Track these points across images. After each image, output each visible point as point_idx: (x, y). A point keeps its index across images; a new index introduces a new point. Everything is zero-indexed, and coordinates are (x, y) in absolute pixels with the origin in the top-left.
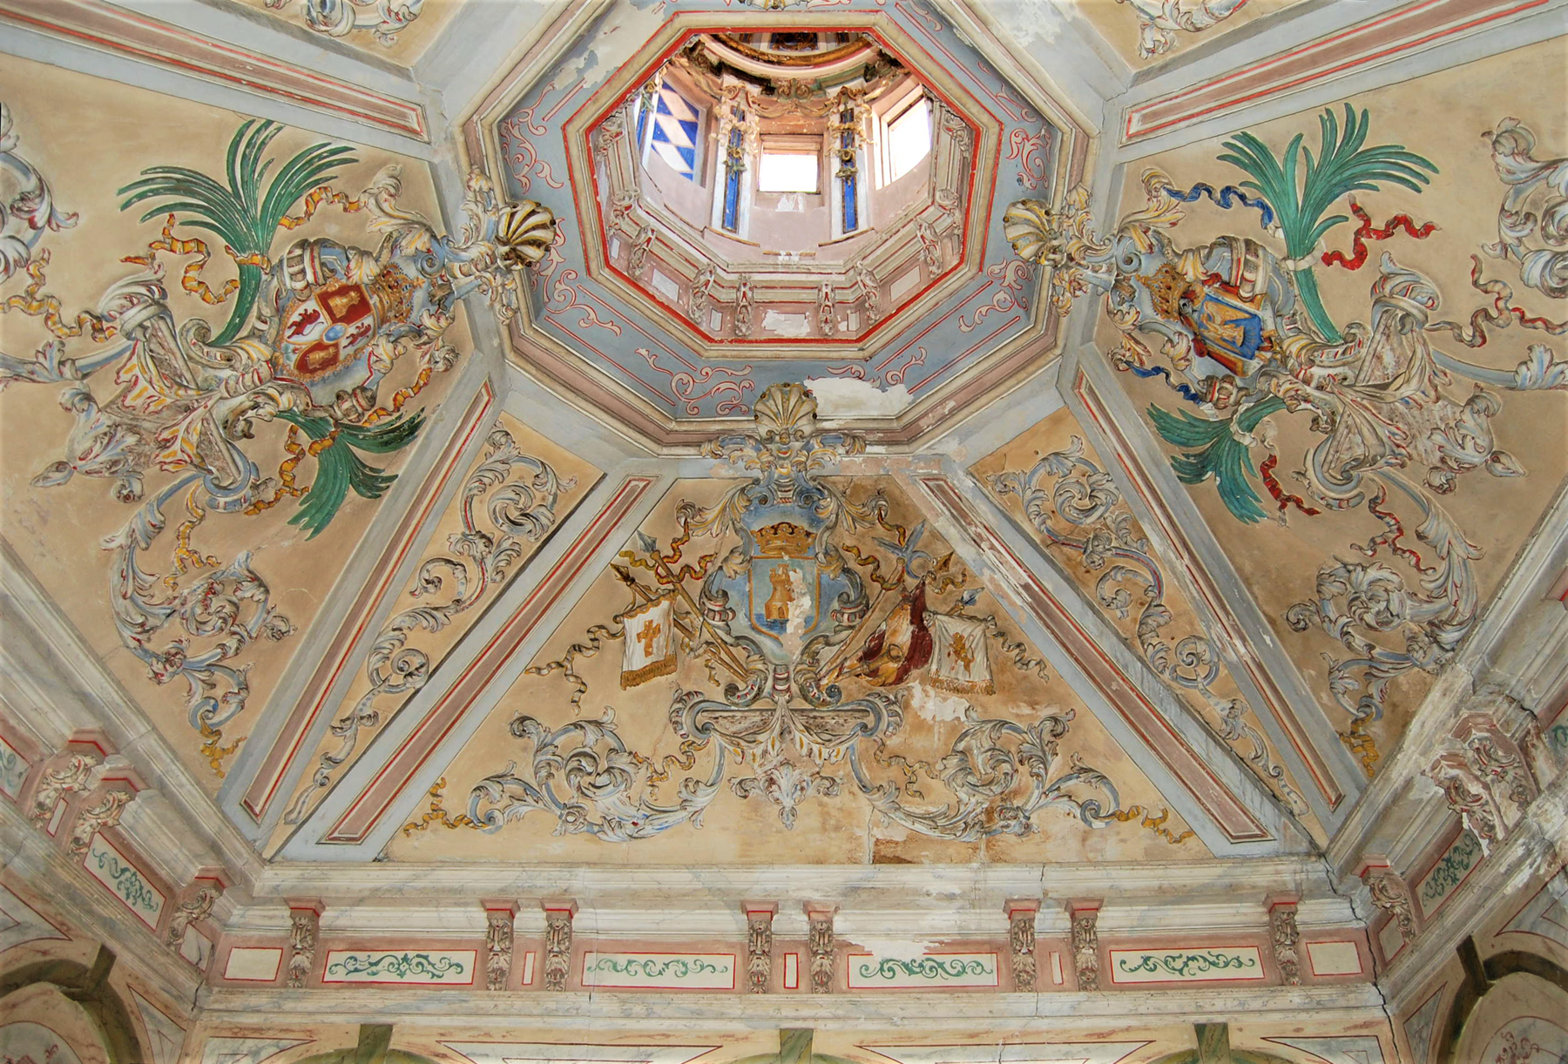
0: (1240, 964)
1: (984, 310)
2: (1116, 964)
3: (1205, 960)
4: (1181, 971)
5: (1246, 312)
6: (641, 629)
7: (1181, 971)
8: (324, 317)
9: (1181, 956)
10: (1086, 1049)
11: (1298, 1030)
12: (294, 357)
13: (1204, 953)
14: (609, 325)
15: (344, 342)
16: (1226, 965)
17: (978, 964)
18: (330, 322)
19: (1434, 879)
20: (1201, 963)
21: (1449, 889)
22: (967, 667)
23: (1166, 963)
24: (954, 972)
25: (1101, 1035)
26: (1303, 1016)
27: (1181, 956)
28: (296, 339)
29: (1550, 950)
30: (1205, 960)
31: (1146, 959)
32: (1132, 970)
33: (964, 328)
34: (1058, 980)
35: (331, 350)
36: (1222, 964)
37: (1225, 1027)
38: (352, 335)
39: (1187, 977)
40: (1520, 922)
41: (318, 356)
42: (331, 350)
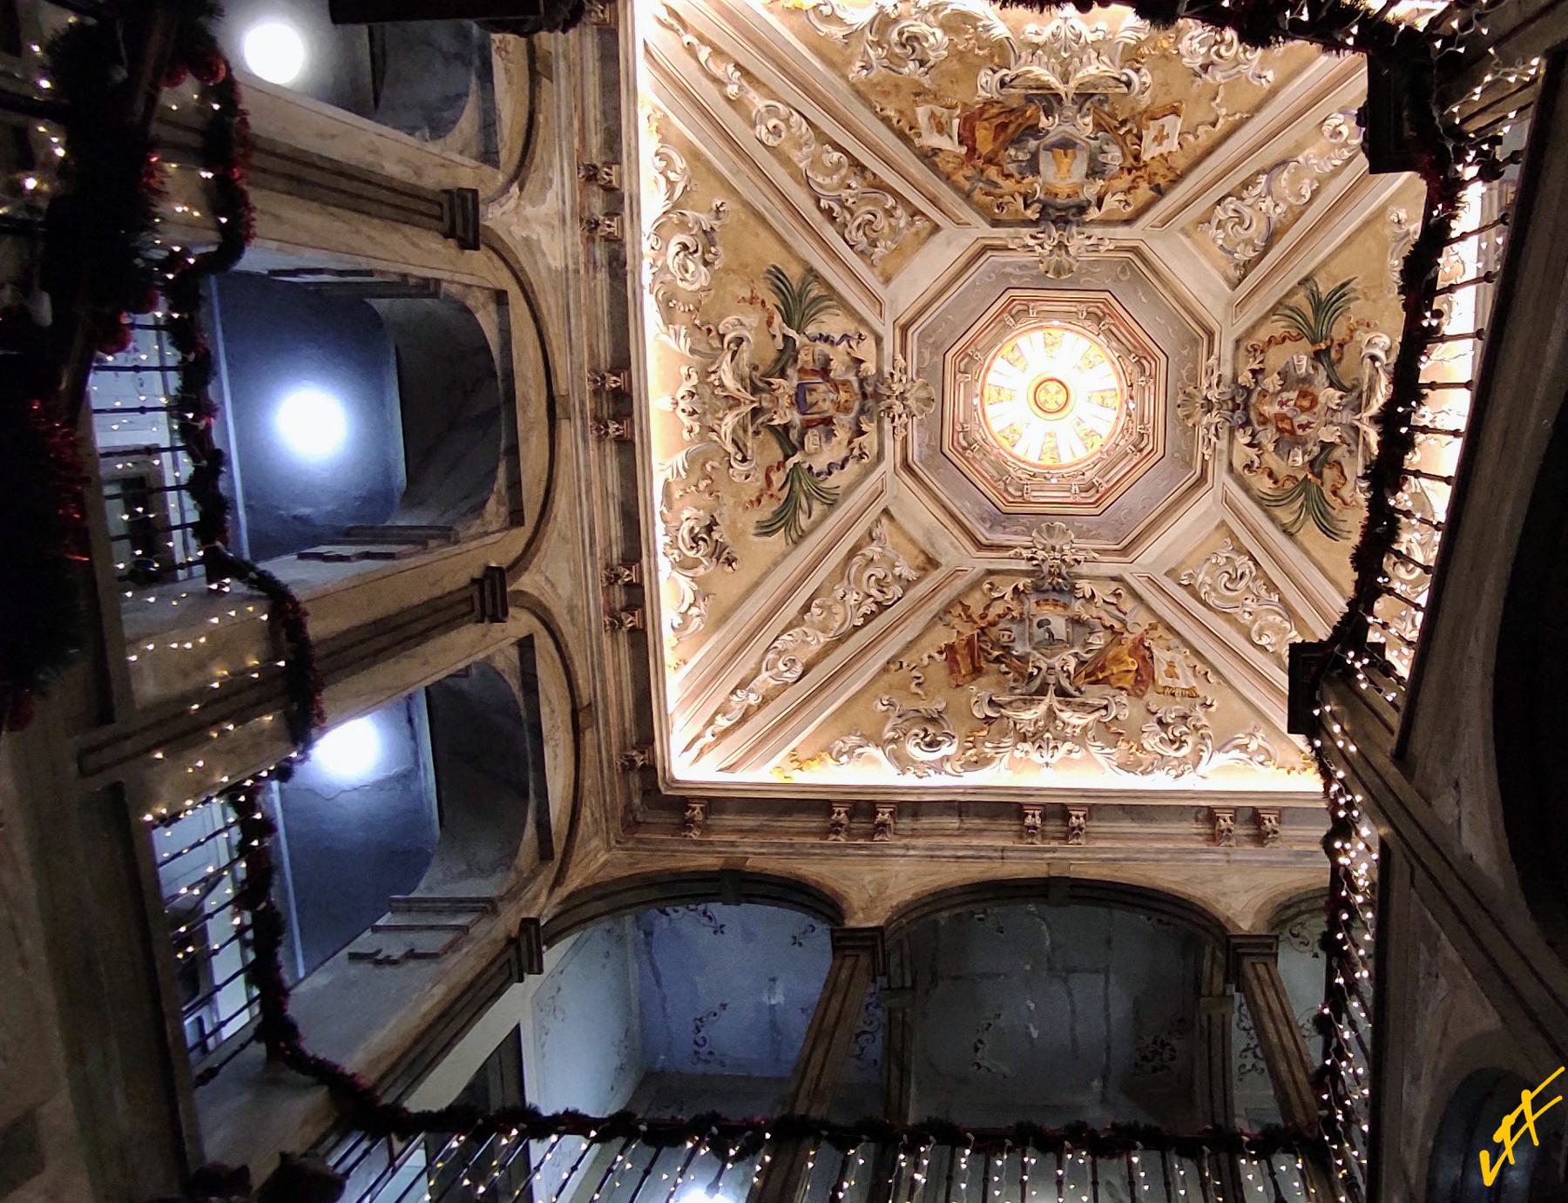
6: (1165, 142)
8: (1296, 424)
12: (1316, 410)
15: (1291, 403)
41: (1306, 403)
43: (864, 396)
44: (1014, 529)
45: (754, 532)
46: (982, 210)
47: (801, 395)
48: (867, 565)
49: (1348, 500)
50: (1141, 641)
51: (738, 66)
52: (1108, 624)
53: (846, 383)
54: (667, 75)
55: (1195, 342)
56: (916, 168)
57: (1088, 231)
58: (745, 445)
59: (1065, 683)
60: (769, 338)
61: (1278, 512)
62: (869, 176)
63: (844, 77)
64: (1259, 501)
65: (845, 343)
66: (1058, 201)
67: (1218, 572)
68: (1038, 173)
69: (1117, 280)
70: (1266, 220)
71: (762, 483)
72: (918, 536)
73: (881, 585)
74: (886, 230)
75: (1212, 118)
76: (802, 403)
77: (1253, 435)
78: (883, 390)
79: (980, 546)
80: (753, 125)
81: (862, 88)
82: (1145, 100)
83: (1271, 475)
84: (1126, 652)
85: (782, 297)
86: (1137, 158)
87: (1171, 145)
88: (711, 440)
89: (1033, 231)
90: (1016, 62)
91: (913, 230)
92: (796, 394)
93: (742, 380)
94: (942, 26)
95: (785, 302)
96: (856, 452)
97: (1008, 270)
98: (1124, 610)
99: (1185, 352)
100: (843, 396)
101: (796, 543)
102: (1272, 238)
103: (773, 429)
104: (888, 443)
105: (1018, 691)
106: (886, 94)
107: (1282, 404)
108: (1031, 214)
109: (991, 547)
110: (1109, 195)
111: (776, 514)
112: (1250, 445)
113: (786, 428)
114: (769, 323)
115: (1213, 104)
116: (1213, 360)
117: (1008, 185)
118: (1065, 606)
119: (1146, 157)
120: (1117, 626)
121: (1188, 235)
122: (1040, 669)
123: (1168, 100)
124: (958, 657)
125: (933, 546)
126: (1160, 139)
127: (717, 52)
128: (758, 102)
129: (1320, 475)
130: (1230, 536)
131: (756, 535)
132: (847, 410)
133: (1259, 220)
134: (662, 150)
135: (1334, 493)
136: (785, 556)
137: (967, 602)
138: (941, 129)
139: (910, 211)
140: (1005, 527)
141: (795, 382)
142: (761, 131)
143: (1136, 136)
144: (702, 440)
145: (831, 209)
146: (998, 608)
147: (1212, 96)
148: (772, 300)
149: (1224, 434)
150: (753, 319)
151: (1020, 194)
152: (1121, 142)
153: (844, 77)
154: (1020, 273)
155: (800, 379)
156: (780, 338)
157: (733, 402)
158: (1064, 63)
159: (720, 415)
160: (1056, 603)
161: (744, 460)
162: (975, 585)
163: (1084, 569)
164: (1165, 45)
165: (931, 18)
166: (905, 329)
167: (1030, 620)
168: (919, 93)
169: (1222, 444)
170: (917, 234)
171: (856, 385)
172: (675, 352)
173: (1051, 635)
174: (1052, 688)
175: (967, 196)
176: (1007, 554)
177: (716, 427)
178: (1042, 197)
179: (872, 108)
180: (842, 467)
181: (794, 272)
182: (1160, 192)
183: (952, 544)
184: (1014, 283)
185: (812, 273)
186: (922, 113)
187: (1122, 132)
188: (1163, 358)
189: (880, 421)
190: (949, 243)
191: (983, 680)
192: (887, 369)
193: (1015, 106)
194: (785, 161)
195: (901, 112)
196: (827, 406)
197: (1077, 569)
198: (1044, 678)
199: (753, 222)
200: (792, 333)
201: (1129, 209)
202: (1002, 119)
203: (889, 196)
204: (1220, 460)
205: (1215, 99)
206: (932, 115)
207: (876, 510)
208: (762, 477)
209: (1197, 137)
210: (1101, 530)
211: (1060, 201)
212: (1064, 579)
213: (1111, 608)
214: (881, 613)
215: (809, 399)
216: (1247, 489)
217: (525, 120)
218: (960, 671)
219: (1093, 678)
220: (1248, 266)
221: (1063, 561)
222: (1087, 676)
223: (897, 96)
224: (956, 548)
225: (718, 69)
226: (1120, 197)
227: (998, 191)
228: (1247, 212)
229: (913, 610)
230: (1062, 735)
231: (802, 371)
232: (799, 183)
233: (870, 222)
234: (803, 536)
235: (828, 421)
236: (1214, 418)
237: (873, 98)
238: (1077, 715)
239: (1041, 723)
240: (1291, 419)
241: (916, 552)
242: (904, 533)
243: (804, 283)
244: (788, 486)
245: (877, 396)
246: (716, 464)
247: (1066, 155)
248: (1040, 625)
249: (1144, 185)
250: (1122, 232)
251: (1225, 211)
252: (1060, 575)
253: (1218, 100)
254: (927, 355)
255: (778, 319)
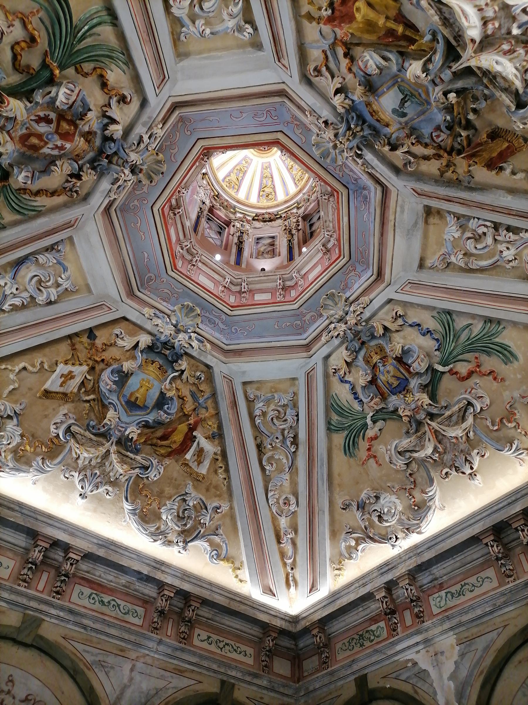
0: (246, 655)
1: (288, 324)
2: (196, 635)
3: (233, 647)
4: (221, 649)
5: (405, 377)
6: (66, 373)
7: (221, 649)
8: (53, 126)
9: (223, 641)
10: (171, 676)
11: (262, 698)
12: (24, 131)
13: (232, 643)
14: (142, 234)
15: (50, 146)
16: (240, 653)
17: (136, 612)
18: (54, 130)
19: (349, 642)
20: (230, 648)
21: (356, 649)
22: (198, 465)
23: (216, 642)
24: (123, 611)
25: (180, 671)
26: (265, 692)
27: (223, 641)
28: (33, 123)
29: (416, 692)
30: (233, 647)
31: (209, 637)
32: (201, 641)
33: (276, 327)
34: (169, 634)
35: (42, 144)
36: (238, 652)
37: (233, 685)
38: (57, 146)
39: (223, 653)
40: (400, 675)
41: (34, 141)
42: (42, 144)
43: (363, 343)
44: (351, 173)
45: (516, 363)
46: (210, 379)
47: (398, 390)
48: (472, 255)
49: (17, 24)
50: (330, 20)
51: (279, 542)
52: (347, 61)
53: (367, 362)
54: (313, 570)
55: (124, 209)
56: (230, 434)
57: (154, 331)
58: (460, 410)
59: (438, 58)
60: (383, 431)
61: (113, 41)
62: (259, 441)
63: (231, 508)
64: (130, 61)
65: (346, 378)
66: (161, 362)
67: (211, 15)
68: (162, 393)
69: (158, 276)
70: (18, 277)
71: (475, 380)
72: (419, 234)
73: (478, 238)
74: (272, 407)
75: (24, 373)
76: (403, 386)
77: (105, 127)
78: (350, 336)
79: (385, 191)
80: (294, 513)
81: (226, 496)
82: (64, 409)
83: (104, 85)
84: (354, 25)
85: (356, 439)
86: (92, 369)
87: (62, 369)
88: (475, 434)
89: (189, 351)
90: (131, 477)
91: (258, 393)
92: (400, 392)
93: (420, 438)
94: (160, 518)
95: (357, 436)
96: (400, 322)
97: (221, 326)
98: (322, 56)
99: (136, 203)
100: (376, 359)
101: (499, 322)
102: (20, 262)
103: (433, 397)
104: (376, 304)
105: (486, 92)
106: (216, 487)
107: (62, 148)
108: (184, 364)
109: (378, 181)
110: (127, 348)
111: (489, 354)
112: (113, 121)
113: (424, 388)
114: (376, 438)
115: (17, 385)
116: (113, 196)
117: (185, 392)
118: (368, 104)
119: (85, 368)
120: (340, 51)
121: (88, 287)
122: (445, 94)
123: (47, 402)
124: (495, 154)
125: (416, 223)
126: (70, 376)
127: (283, 555)
128: (283, 522)
129: (44, 65)
130: (179, 39)
131: (516, 358)
132: (381, 349)
133: (24, 277)
134: (347, 555)
135: (33, 40)
136: (515, 324)
137: (438, 173)
138: (200, 452)
139: (252, 404)
140: (356, 180)
141: (394, 397)
142: (293, 508)
143: (84, 387)
144: (480, 441)
145: (292, 443)
146: (419, 150)
147: (14, 392)
148: (363, 445)
149: (133, 137)
150: (380, 449)
151: (182, 380)
152: (96, 389)
153: (231, 508)
154: (217, 321)
155: (389, 395)
156: (380, 424)
157: (439, 437)
158: (101, 465)
159: (454, 440)
160: (373, 113)
161: (470, 404)
162: (419, 176)
163: (326, 113)
164: (28, 448)
165: (163, 527)
166: (307, 347)
167: (406, 123)
168: (197, 479)
169: (140, 130)
170: (258, 389)
171: (362, 353)
172: (441, 490)
173: (403, 102)
174: (456, 67)
175: (214, 395)
176: (373, 172)
177: (464, 438)
178: (170, 371)
179: (229, 483)
180: (419, 325)
181: (339, 439)
182: (91, 333)
183: (402, 212)
184: (224, 317)
185: (330, 428)
186: (203, 470)
187: (92, 397)
188: (155, 209)
189: (367, 321)
190: (244, 373)
191: (501, 123)
192: (336, 342)
193: (149, 447)
194: (294, 484)
195: (216, 472)
196: (390, 368)
197: (332, 119)
198: (451, 81)
199: (336, 481)
200: (369, 421)
201: (117, 331)
202: (160, 443)
203: (257, 423)
204: (150, 118)
205: (13, 389)
206: (199, 463)
207: (425, 277)
208: (471, 382)
209: (42, 363)
210: (290, 120)
211: (160, 361)
212: (348, 122)
213: (332, 65)
214: (500, 224)
215: (396, 383)
216: (136, 79)
217: (385, 227)
218: (508, 147)
219: (408, 33)
220: (50, 249)
221: (336, 135)
222: (412, 41)
223: (211, 484)
224: (402, 207)
225: (289, 549)
226: (120, 342)
227: (194, 389)
228: (32, 288)
229: (481, 206)
230: (502, 14)
231: (384, 398)
232: (297, 469)
233: (278, 418)
234: (489, 320)
235: (399, 360)
236: (133, 157)
237: (225, 488)
238: (465, 23)
239: (506, 47)
240: (57, 132)
241: (431, 228)
242: (424, 247)
243: (339, 430)
244: (460, 357)
245: (356, 334)
246: (489, 423)
247: (137, 398)
248: (404, 115)
249: (99, 342)
250: (133, 316)
251: (49, 294)
252: (349, 128)
253: (12, 387)
254: (308, 317)
255: (370, 433)
